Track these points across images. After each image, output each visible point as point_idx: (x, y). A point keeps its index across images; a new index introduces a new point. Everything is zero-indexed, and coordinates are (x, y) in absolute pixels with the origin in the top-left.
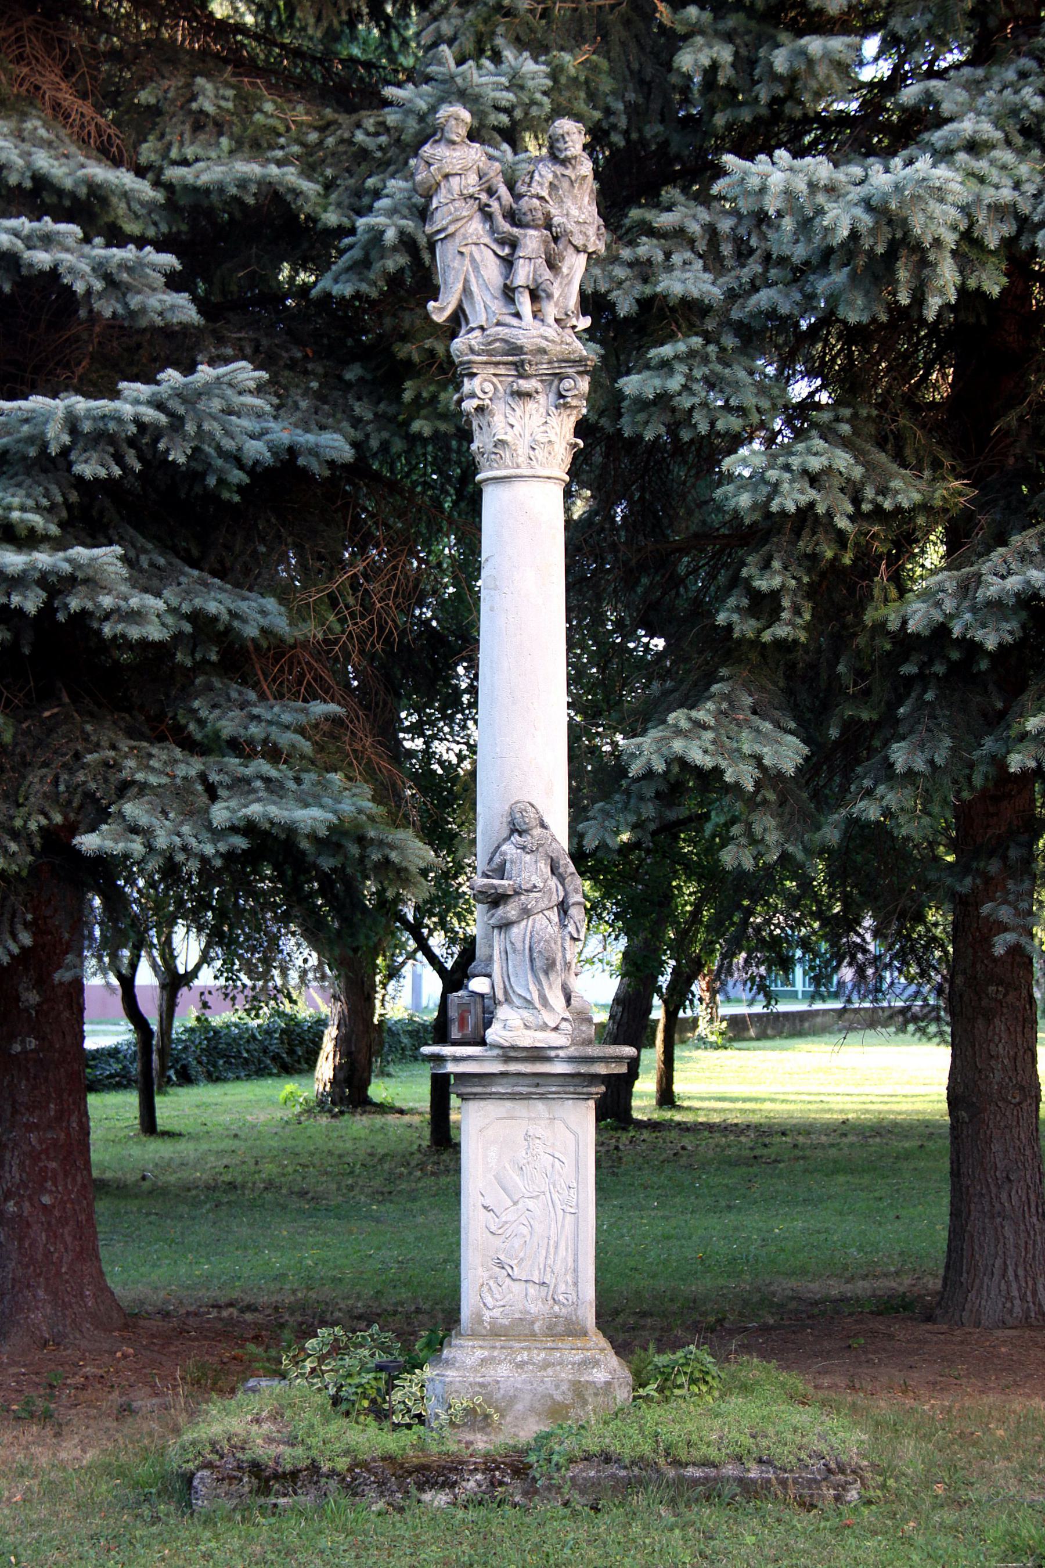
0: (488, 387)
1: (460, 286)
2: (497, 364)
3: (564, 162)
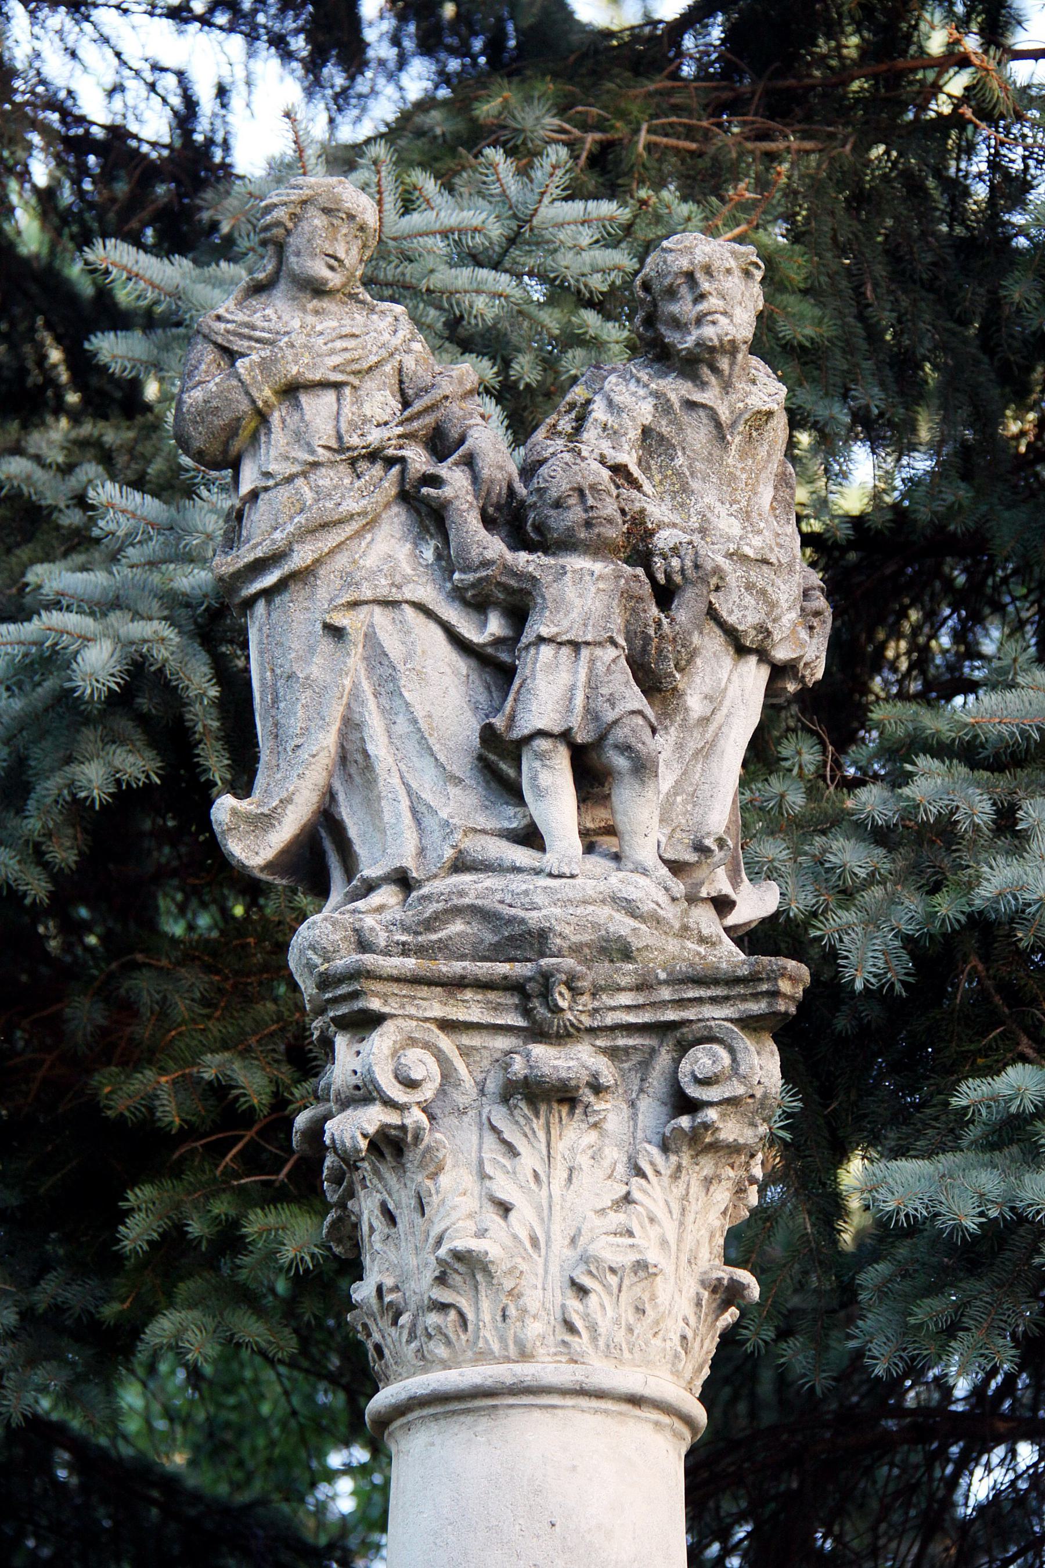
0: (422, 1065)
1: (328, 740)
2: (455, 985)
3: (692, 364)
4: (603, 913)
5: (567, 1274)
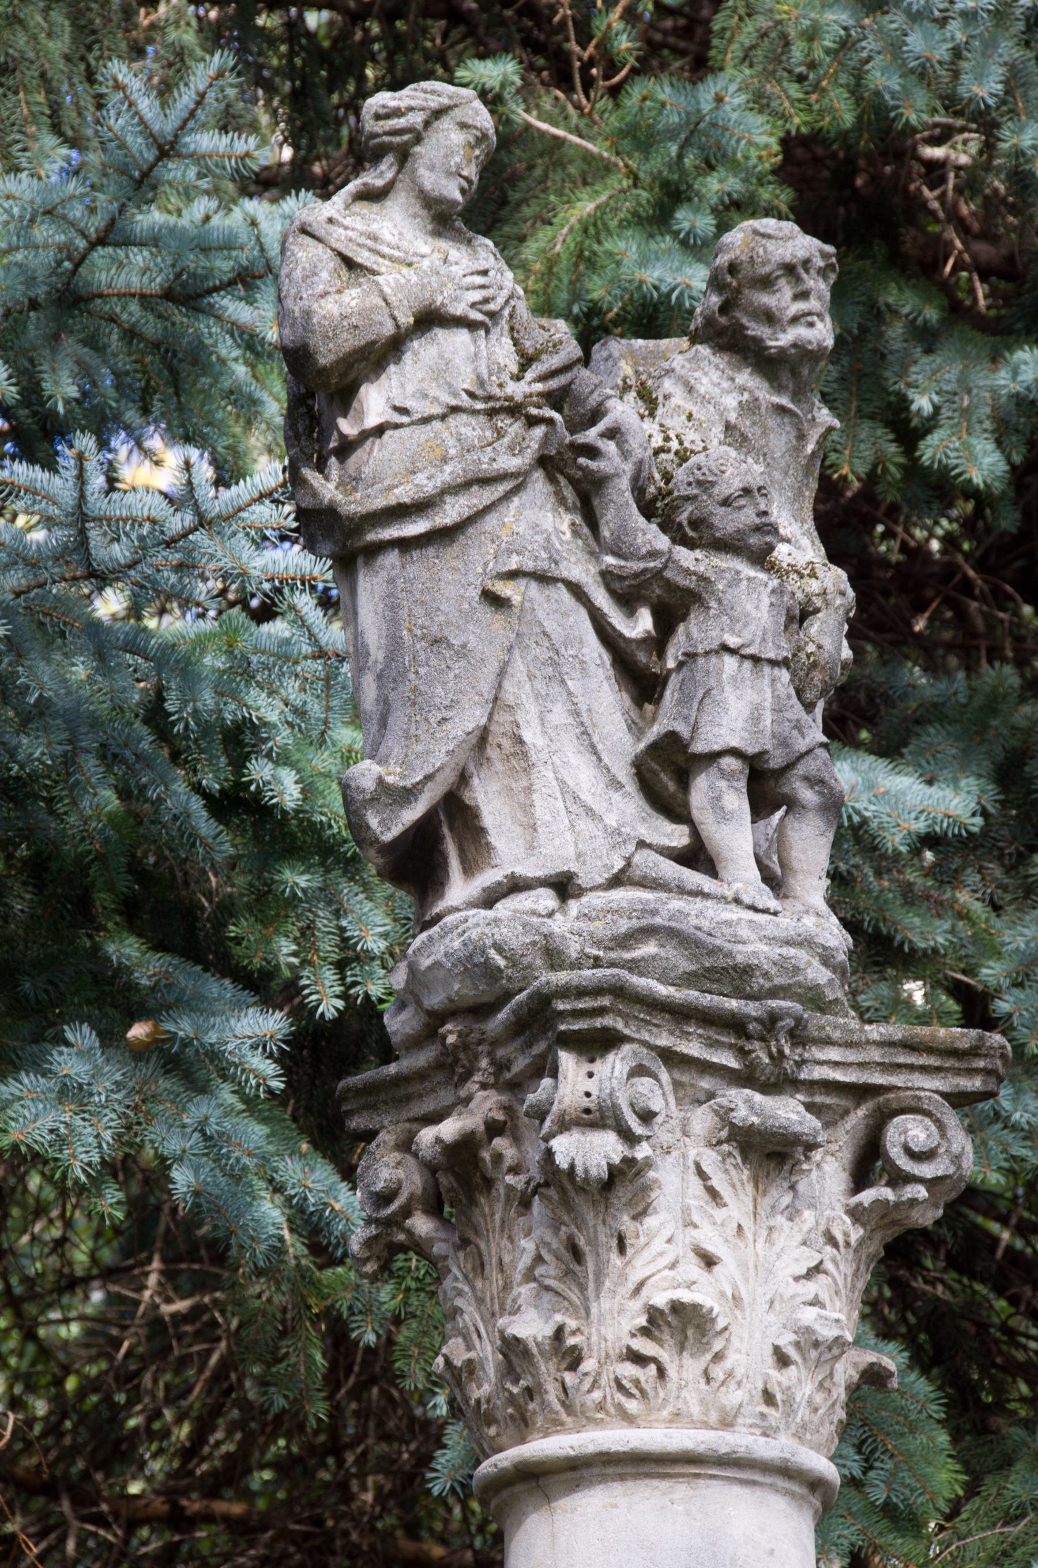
4: (801, 956)
5: (770, 1341)
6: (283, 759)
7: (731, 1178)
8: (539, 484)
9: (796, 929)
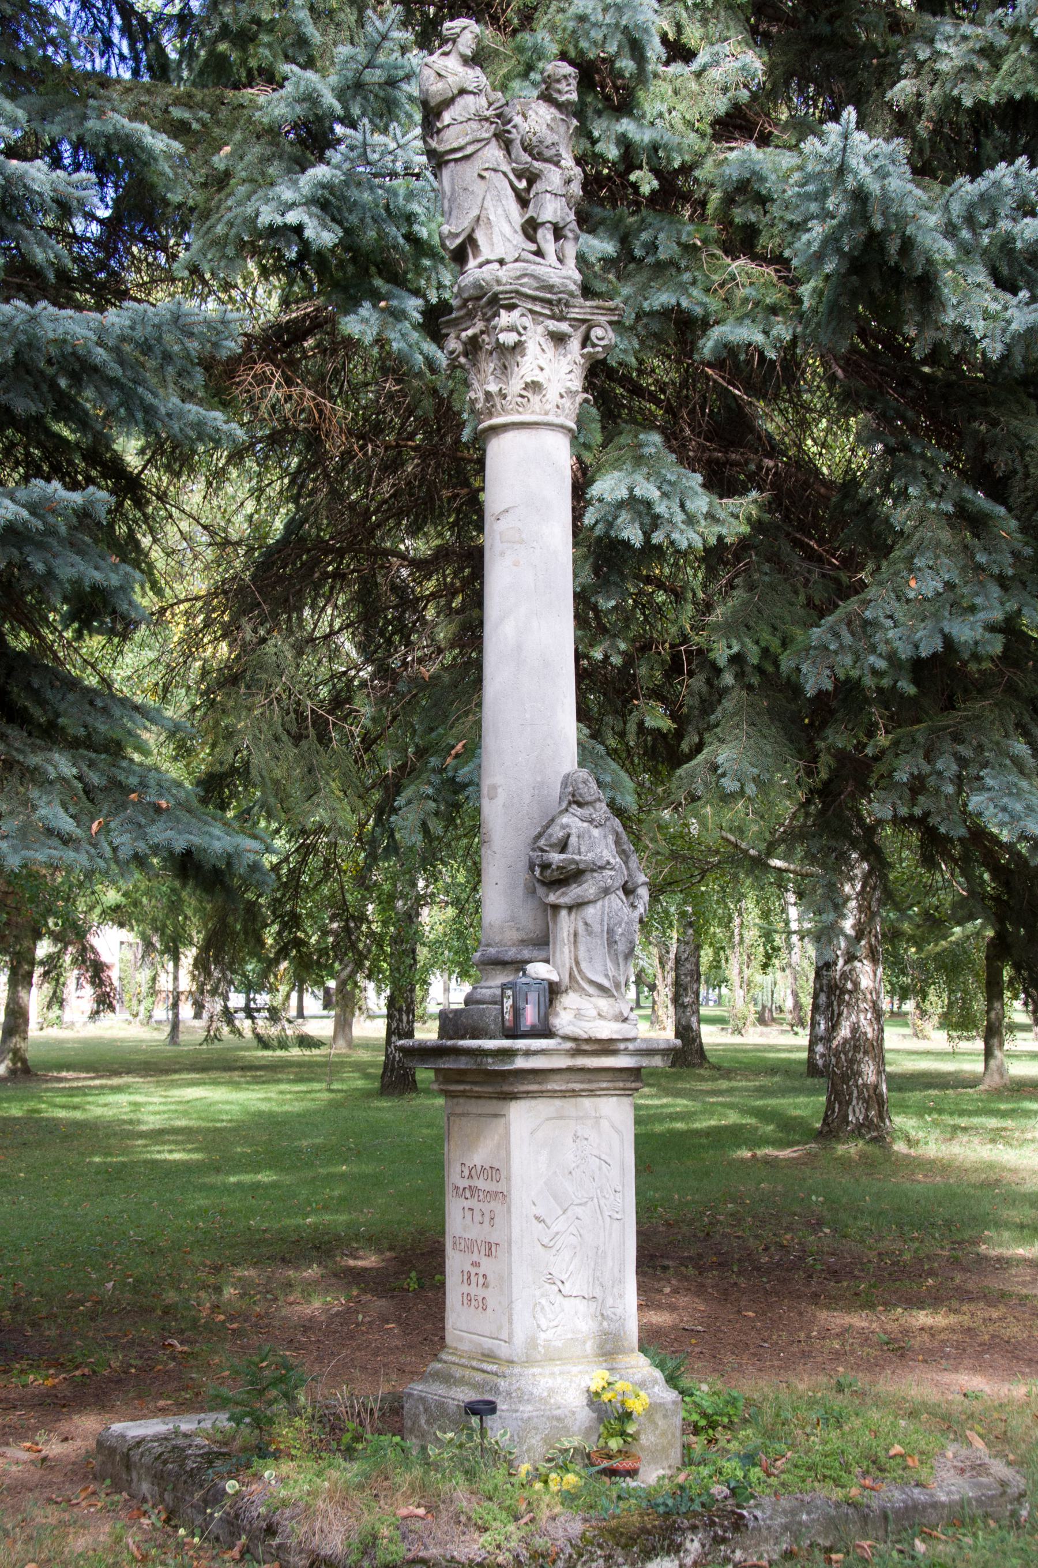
6: (422, 224)
7: (549, 346)
8: (494, 141)
9: (568, 275)
